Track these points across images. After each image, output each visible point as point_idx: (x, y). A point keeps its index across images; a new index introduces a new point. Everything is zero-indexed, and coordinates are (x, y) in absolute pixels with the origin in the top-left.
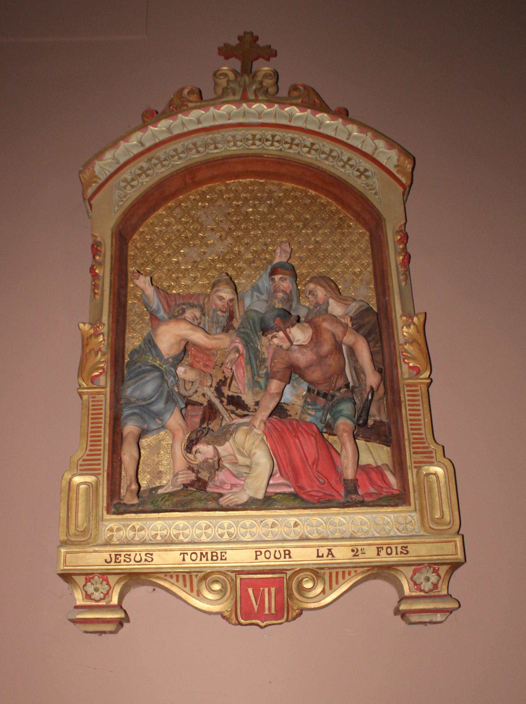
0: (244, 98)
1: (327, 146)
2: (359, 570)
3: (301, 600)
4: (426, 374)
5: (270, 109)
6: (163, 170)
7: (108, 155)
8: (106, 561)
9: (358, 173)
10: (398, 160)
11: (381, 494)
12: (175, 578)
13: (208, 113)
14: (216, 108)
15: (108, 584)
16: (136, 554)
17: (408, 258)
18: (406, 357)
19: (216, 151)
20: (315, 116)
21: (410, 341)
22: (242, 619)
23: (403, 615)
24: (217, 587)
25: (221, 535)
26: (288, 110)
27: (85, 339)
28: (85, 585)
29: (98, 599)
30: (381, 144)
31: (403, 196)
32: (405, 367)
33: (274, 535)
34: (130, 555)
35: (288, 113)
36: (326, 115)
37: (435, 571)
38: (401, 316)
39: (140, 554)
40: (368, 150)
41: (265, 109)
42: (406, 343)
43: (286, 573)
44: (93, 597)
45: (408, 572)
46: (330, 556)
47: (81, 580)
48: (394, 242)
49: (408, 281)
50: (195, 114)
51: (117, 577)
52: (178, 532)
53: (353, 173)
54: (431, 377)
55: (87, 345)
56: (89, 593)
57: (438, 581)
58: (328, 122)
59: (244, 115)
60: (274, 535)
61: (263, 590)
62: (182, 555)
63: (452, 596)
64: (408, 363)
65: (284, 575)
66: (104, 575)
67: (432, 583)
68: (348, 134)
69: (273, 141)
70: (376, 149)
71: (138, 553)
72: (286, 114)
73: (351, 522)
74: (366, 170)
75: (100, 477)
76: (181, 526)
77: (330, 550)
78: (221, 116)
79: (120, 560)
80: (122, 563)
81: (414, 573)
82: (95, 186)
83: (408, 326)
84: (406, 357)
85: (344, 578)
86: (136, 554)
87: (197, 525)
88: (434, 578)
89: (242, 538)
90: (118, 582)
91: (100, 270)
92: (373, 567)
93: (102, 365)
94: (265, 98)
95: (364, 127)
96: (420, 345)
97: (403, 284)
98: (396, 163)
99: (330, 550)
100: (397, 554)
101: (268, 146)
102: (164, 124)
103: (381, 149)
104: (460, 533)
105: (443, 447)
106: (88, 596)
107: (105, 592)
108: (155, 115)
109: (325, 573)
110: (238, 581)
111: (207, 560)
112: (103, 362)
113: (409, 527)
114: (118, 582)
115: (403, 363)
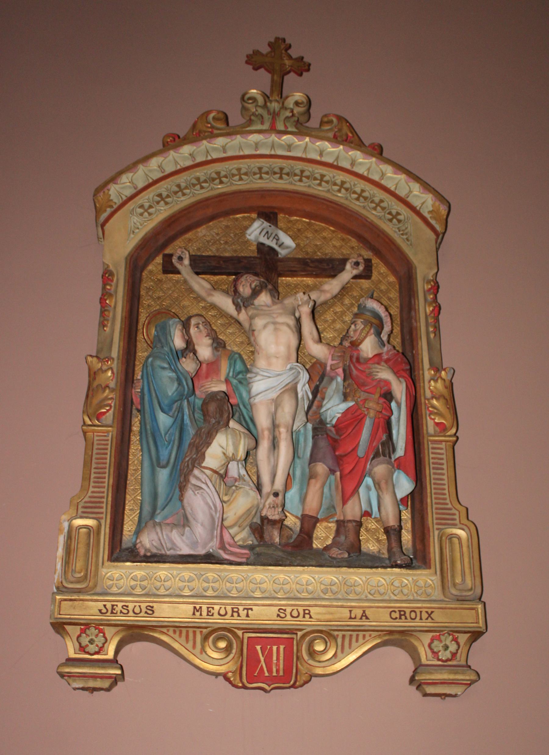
0: (273, 129)
1: (361, 185)
2: (374, 634)
3: (312, 665)
4: (453, 431)
5: (301, 143)
6: (183, 198)
7: (125, 179)
8: (100, 611)
9: (390, 217)
10: (433, 206)
11: (160, 550)
12: (178, 633)
13: (234, 142)
14: (242, 137)
15: (104, 636)
16: (221, 608)
17: (438, 309)
18: (431, 413)
19: (240, 183)
20: (347, 153)
21: (437, 396)
22: (291, 681)
23: (62, 675)
24: (222, 644)
25: (133, 588)
26: (319, 145)
27: (92, 373)
28: (79, 636)
29: (92, 652)
30: (416, 188)
31: (436, 243)
32: (431, 424)
33: (143, 588)
34: (285, 610)
35: (318, 147)
36: (359, 152)
37: (455, 640)
38: (429, 369)
39: (225, 608)
40: (402, 193)
41: (296, 142)
42: (432, 398)
43: (296, 634)
44: (87, 650)
45: (426, 638)
46: (430, 619)
47: (74, 631)
48: (424, 292)
49: (437, 332)
50: (220, 141)
51: (113, 630)
52: (135, 583)
53: (384, 216)
54: (457, 435)
55: (95, 379)
56: (83, 644)
57: (457, 650)
58: (361, 160)
59: (273, 147)
60: (215, 590)
61: (271, 649)
62: (246, 611)
63: (472, 668)
64: (434, 419)
65: (294, 636)
66: (99, 626)
67: (451, 652)
68: (381, 174)
69: (301, 176)
70: (410, 192)
71: (223, 607)
72: (317, 148)
73: (343, 583)
74: (398, 214)
75: (103, 522)
76: (211, 578)
77: (364, 612)
78: (281, 146)
79: (117, 611)
80: (119, 614)
81: (432, 640)
82: (109, 210)
83: (436, 381)
84: (431, 413)
85: (357, 641)
86: (221, 608)
87: (132, 575)
88: (453, 647)
89: (252, 594)
90: (116, 633)
91: (110, 301)
92: (391, 632)
93: (110, 402)
94: (294, 130)
95: (399, 168)
96: (446, 400)
97: (432, 336)
98: (431, 209)
99: (364, 612)
100: (421, 619)
101: (295, 181)
102: (186, 149)
103: (415, 193)
104: (482, 600)
105: (467, 509)
106: (82, 649)
107: (100, 645)
108: (177, 140)
109: (338, 635)
110: (245, 641)
111: (406, 618)
112: (112, 398)
113: (405, 591)
114: (116, 633)
115: (428, 418)
